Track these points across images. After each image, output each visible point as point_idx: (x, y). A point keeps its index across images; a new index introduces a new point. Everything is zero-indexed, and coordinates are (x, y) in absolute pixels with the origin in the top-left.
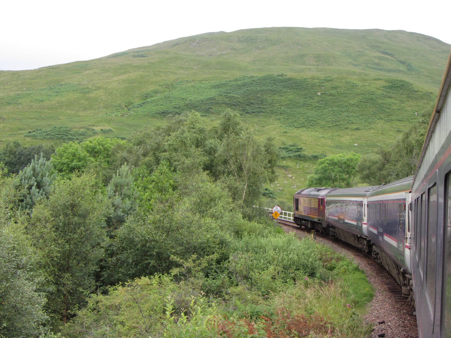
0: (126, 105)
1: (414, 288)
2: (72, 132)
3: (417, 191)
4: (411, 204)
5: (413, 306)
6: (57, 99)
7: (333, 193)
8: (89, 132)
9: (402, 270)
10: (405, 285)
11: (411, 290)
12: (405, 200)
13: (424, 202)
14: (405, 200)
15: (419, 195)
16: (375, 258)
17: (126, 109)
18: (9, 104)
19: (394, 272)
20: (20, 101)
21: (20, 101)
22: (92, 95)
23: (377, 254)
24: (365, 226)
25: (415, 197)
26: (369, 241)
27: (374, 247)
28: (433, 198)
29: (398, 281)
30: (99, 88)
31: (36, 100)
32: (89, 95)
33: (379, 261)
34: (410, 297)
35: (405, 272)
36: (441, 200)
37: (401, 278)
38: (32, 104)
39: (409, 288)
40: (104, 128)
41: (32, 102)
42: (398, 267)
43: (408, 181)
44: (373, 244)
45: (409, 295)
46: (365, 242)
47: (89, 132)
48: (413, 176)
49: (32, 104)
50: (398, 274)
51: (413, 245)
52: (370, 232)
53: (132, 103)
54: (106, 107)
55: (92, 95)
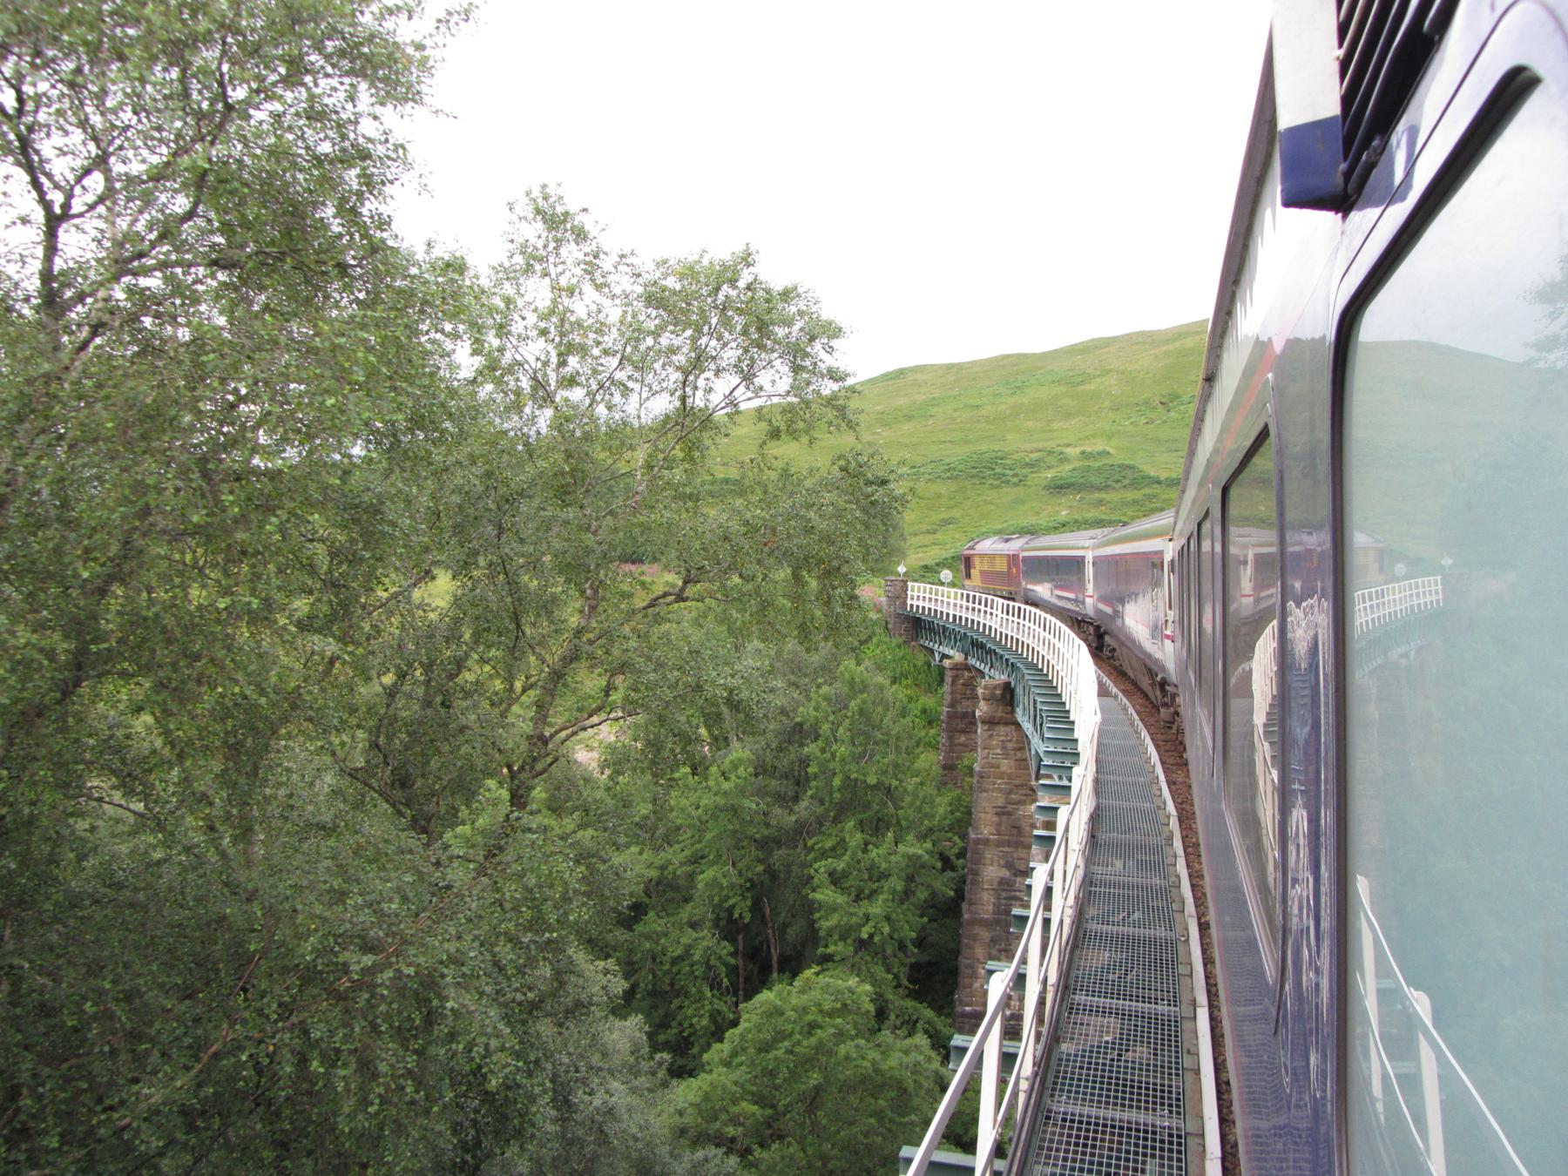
0: (1164, 400)
1: (1182, 710)
2: (1008, 462)
3: (1181, 534)
4: (1172, 561)
5: (1181, 743)
6: (1011, 400)
7: (1033, 544)
8: (1048, 459)
9: (1159, 679)
10: (1165, 705)
11: (1177, 713)
12: (1161, 552)
13: (1192, 556)
14: (1161, 552)
15: (1183, 541)
16: (1109, 658)
17: (1160, 408)
18: (909, 418)
19: (1145, 683)
20: (933, 411)
21: (933, 411)
22: (1090, 387)
23: (1114, 650)
24: (1089, 601)
25: (1179, 548)
26: (1098, 627)
27: (1107, 638)
28: (1206, 546)
29: (1153, 698)
30: (1110, 371)
31: (966, 406)
32: (1082, 387)
33: (1117, 663)
34: (1175, 727)
35: (1163, 684)
36: (1218, 548)
37: (1158, 693)
38: (955, 415)
39: (1172, 709)
40: (1089, 449)
41: (955, 410)
42: (1151, 673)
43: (1164, 520)
44: (1106, 633)
45: (1173, 723)
46: (1091, 630)
47: (1048, 459)
48: (1173, 510)
49: (955, 415)
50: (1153, 685)
51: (1177, 633)
52: (1098, 611)
53: (1178, 397)
54: (1115, 409)
55: (1090, 387)
